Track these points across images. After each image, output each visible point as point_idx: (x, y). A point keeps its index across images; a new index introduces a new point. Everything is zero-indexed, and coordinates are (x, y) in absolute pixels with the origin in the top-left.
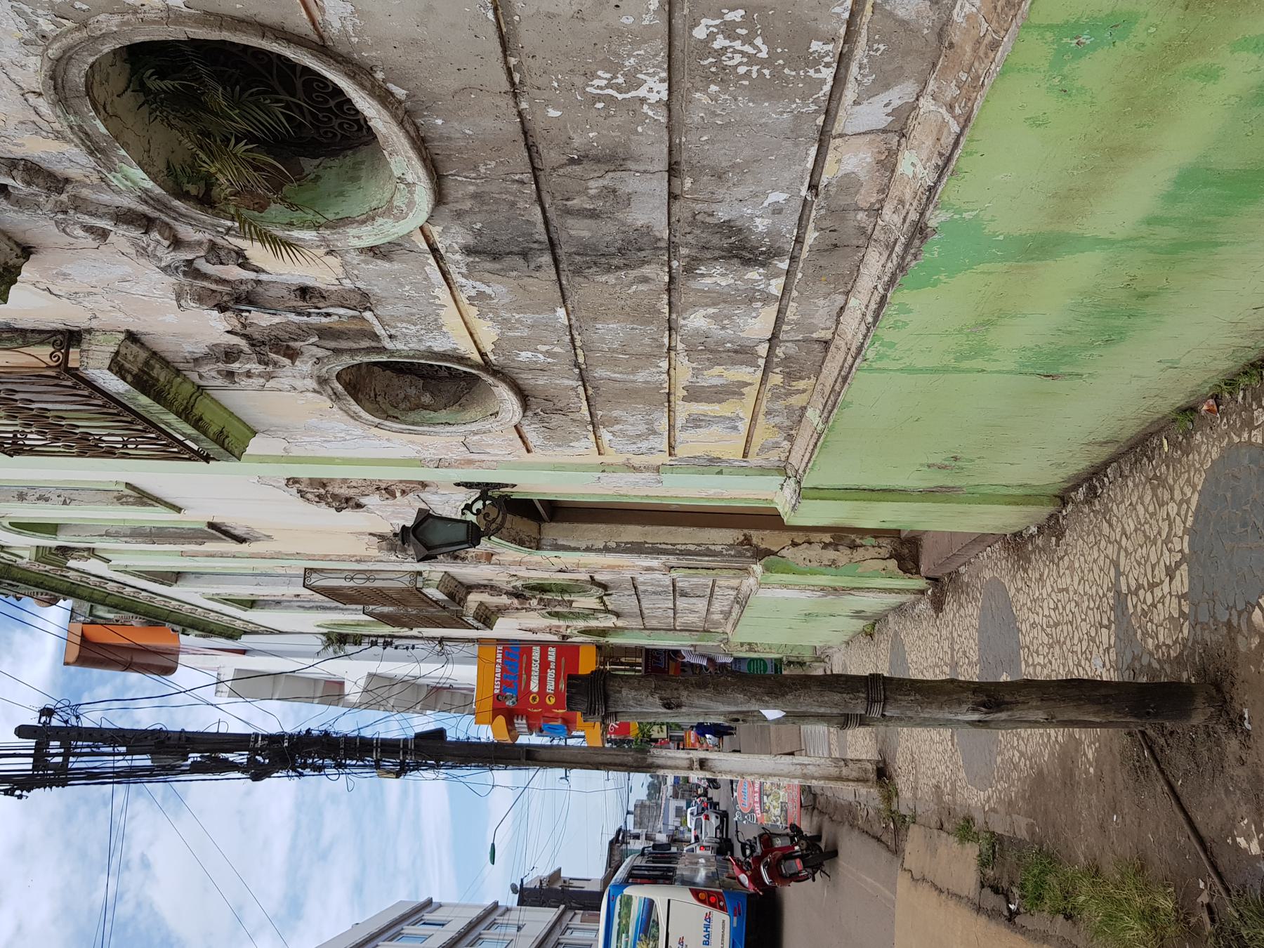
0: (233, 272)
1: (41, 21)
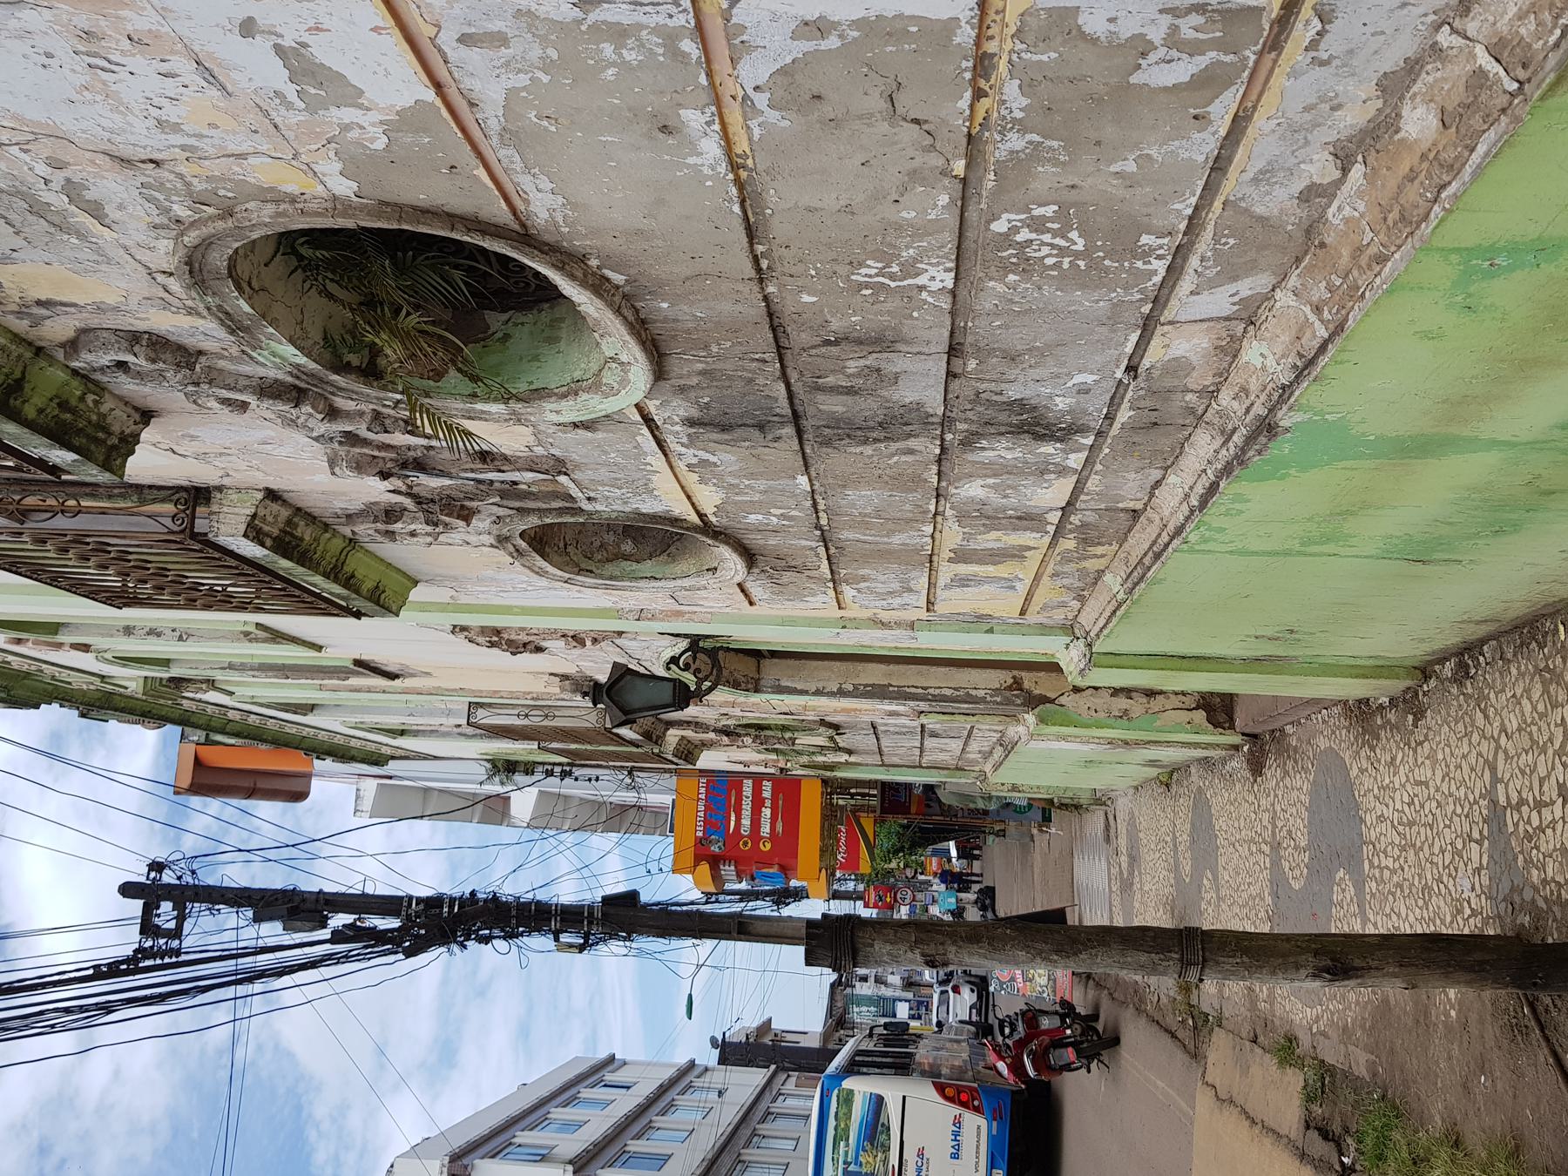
1: (175, 207)
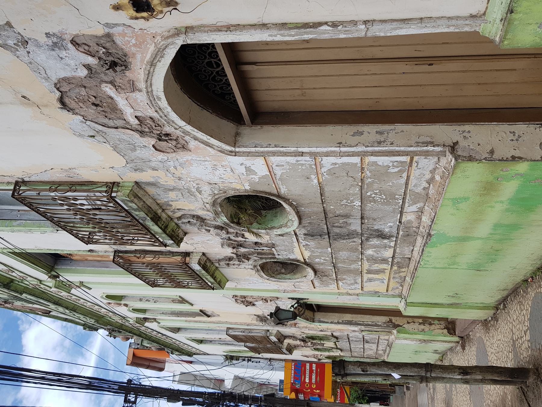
0: (240, 239)
